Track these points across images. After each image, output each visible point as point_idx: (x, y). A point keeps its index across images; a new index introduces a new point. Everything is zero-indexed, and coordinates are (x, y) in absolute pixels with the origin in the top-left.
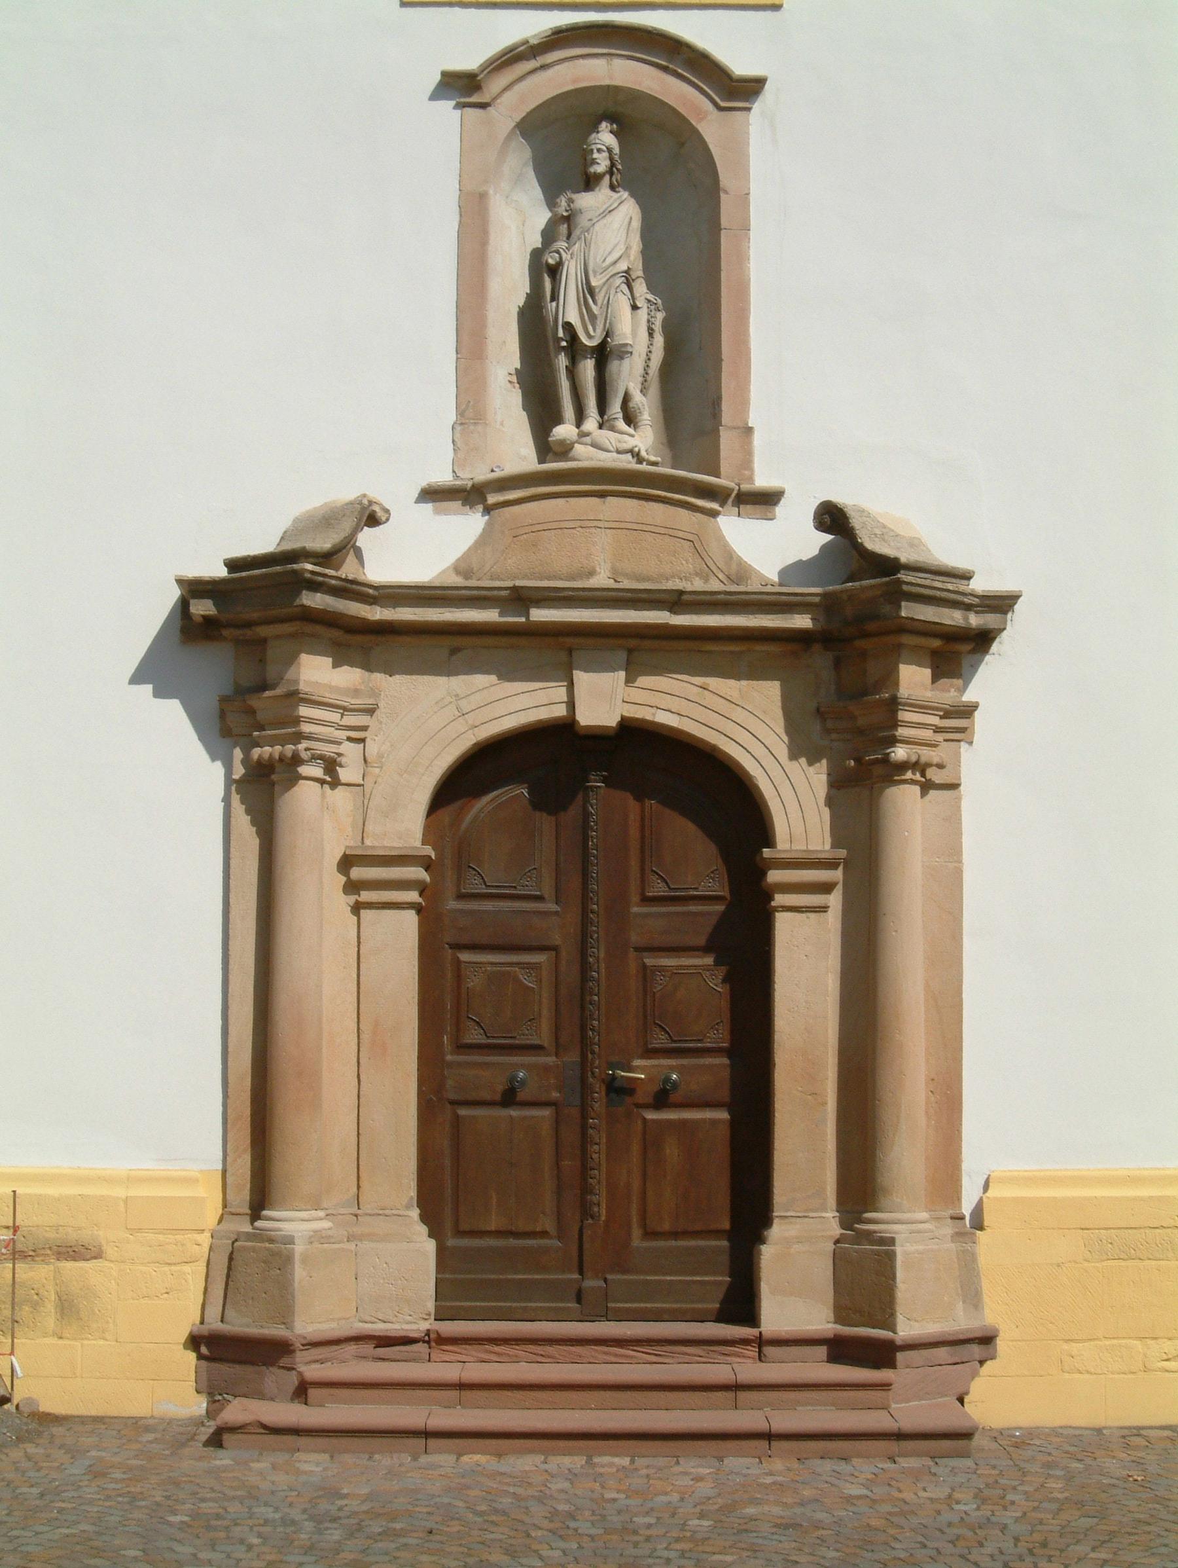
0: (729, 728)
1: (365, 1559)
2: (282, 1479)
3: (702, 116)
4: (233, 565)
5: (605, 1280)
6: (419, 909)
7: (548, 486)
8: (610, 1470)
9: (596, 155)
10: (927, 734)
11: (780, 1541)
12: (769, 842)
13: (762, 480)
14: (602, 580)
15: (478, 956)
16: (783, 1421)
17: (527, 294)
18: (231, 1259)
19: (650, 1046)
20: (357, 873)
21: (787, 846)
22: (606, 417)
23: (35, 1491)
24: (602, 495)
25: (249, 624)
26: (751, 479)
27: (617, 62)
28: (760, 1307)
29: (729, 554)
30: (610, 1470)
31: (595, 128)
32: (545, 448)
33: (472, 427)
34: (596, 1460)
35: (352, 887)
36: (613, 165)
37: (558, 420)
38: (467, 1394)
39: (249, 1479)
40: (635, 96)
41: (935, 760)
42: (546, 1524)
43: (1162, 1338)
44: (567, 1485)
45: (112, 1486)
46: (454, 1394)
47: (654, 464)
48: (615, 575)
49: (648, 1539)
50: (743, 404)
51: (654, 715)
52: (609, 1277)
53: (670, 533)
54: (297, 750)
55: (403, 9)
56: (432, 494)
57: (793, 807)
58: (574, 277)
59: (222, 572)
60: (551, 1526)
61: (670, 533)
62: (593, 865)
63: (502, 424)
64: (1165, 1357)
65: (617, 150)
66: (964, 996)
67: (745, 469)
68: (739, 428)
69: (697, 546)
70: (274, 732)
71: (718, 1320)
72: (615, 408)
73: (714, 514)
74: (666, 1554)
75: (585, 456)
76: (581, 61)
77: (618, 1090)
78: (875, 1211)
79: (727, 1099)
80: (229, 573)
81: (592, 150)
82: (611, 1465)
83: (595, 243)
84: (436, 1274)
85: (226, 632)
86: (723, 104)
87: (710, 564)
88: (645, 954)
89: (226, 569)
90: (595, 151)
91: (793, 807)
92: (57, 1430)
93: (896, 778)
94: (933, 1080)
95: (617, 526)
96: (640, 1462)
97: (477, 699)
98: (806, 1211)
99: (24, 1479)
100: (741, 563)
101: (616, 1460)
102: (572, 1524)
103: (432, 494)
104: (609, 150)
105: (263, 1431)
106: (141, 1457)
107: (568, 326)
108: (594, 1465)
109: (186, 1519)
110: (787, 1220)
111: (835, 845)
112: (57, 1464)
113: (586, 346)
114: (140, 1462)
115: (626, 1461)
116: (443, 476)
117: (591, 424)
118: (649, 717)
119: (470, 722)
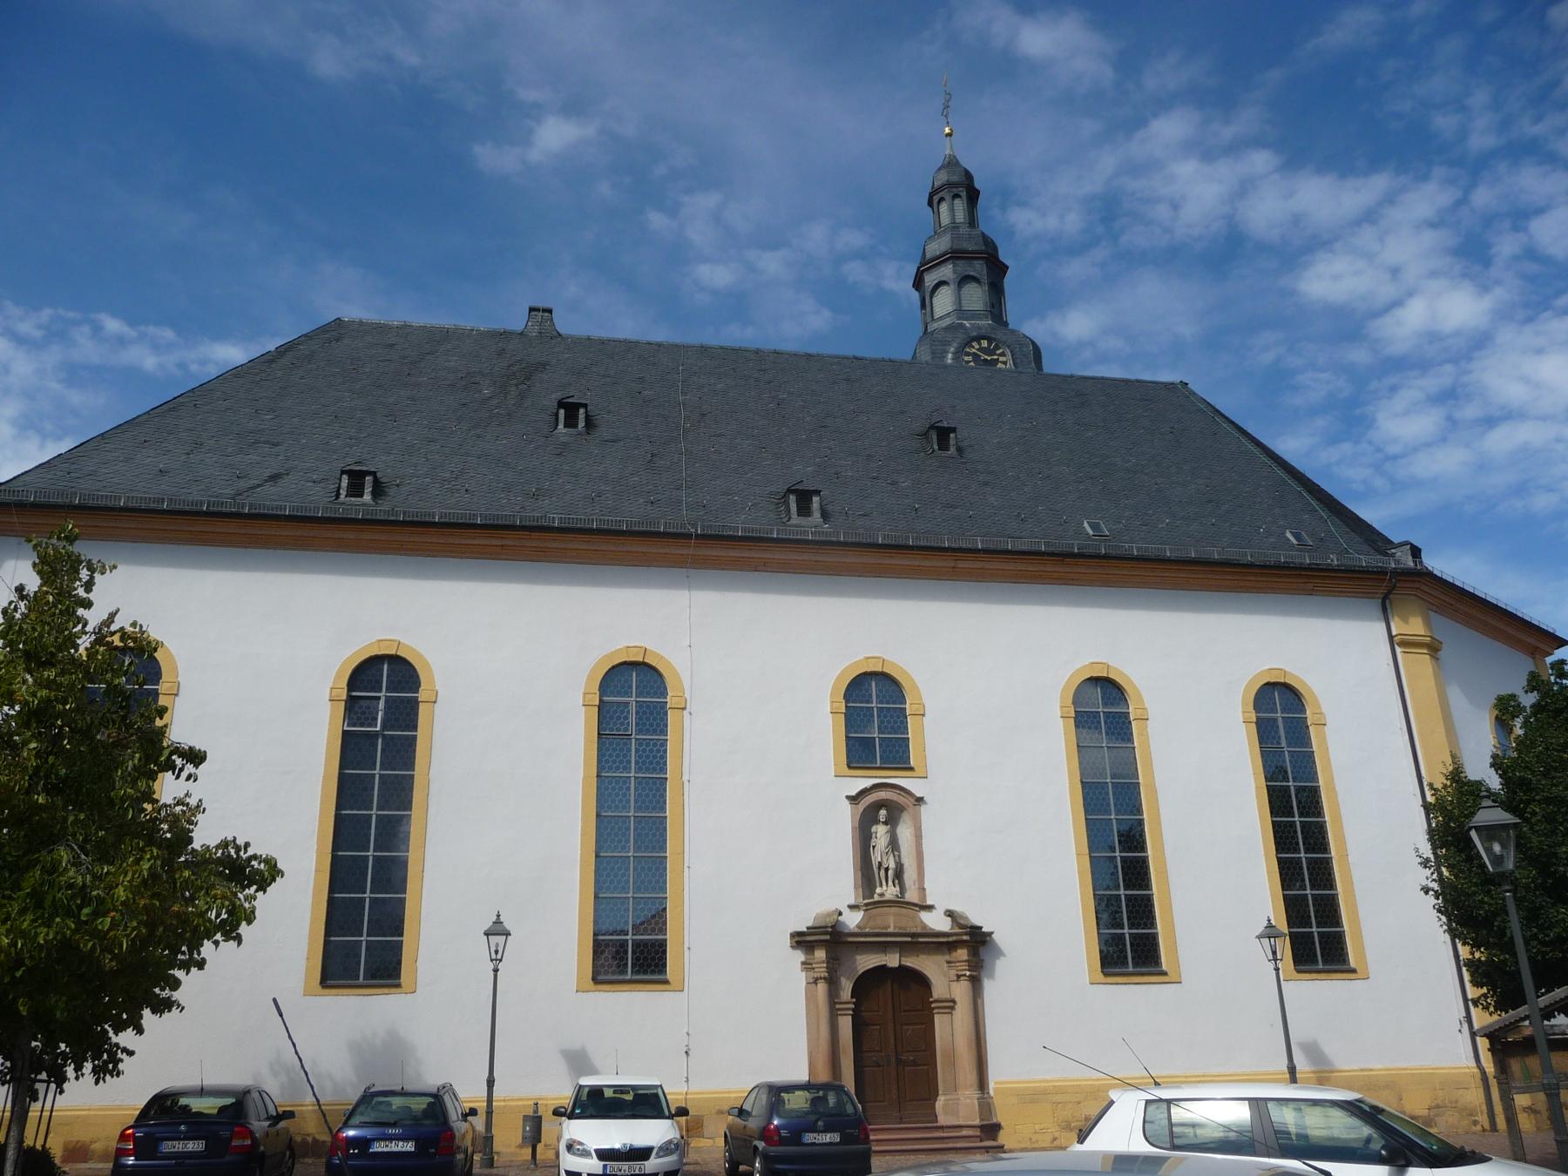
4: (808, 928)
13: (929, 902)
14: (891, 930)
16: (958, 1145)
17: (981, 928)
22: (337, 485)
24: (890, 906)
26: (926, 902)
29: (922, 922)
56: (851, 907)
84: (1283, 889)
97: (864, 960)
111: (852, 997)
116: (852, 902)
117: (884, 888)
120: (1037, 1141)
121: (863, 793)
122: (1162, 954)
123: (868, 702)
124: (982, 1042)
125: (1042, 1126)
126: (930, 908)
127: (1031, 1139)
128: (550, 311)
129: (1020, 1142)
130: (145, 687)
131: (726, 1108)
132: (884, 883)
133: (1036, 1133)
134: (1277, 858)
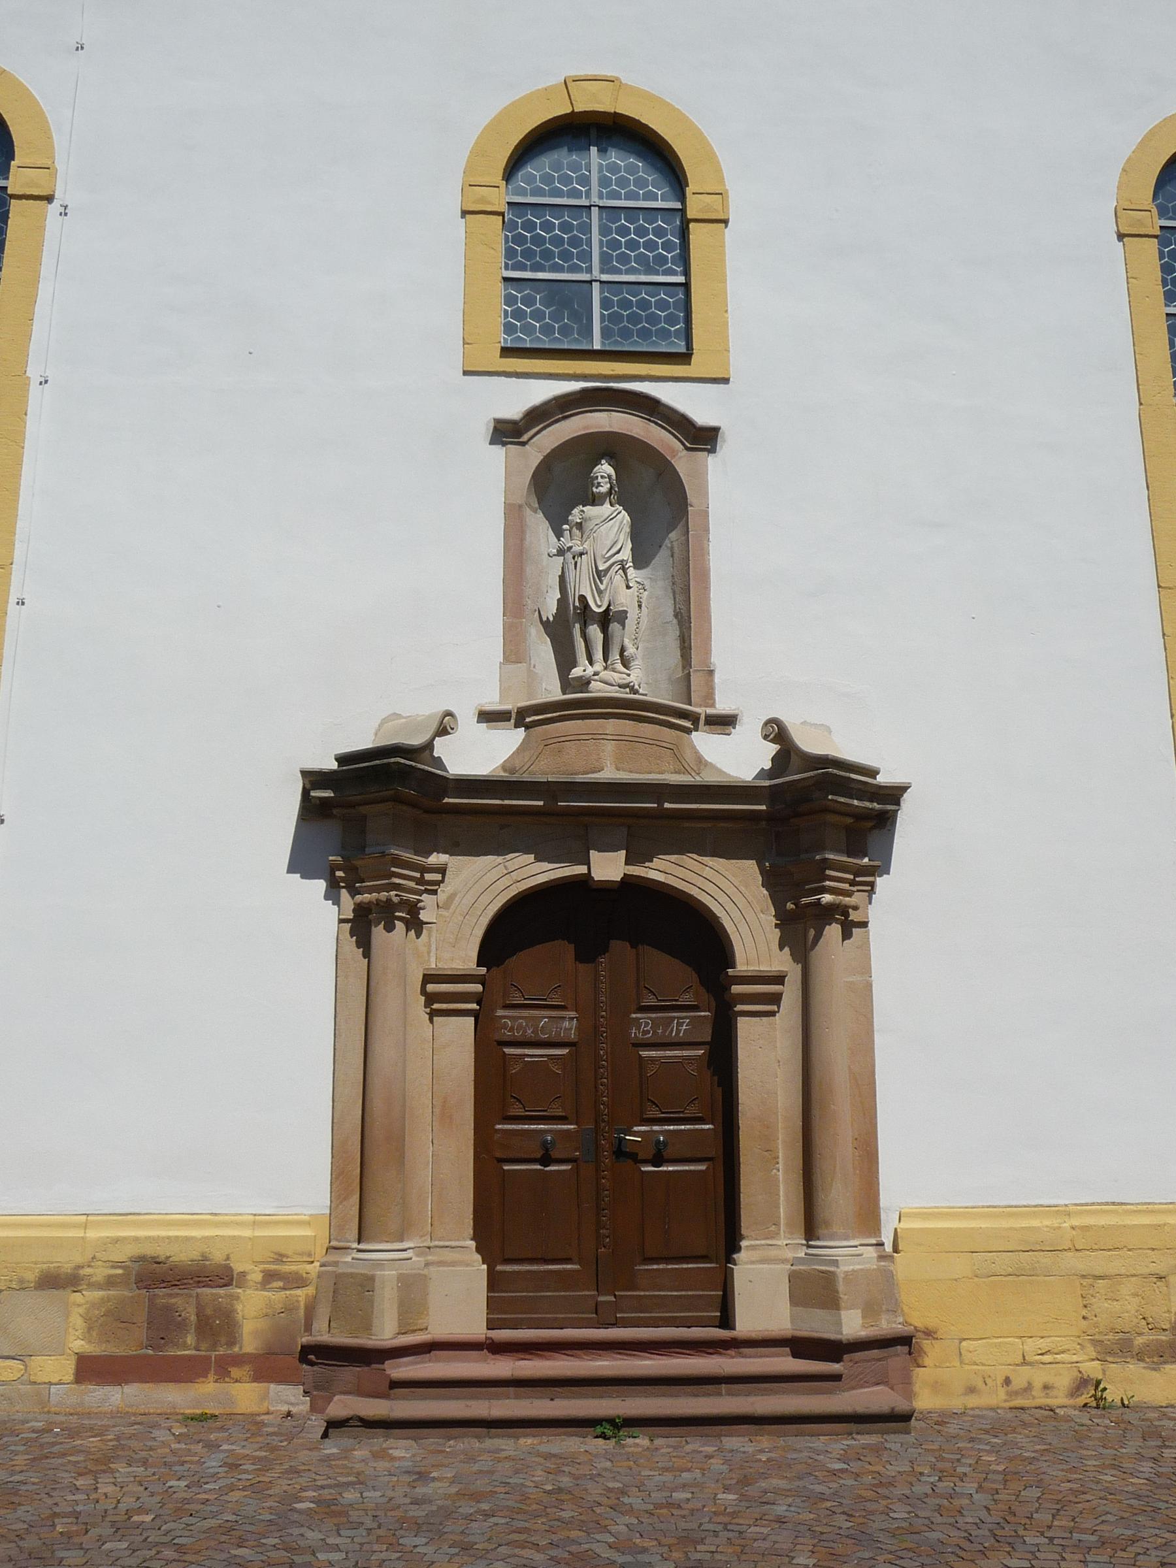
0: (700, 882)
1: (465, 1540)
3: (674, 453)
4: (342, 759)
5: (615, 1296)
6: (476, 1015)
9: (600, 480)
10: (846, 886)
11: (799, 1513)
12: (733, 966)
13: (722, 706)
15: (551, 1050)
19: (645, 1116)
20: (431, 987)
21: (744, 968)
22: (609, 662)
23: (183, 1483)
25: (352, 806)
31: (598, 463)
32: (567, 684)
35: (430, 999)
36: (611, 488)
37: (574, 664)
39: (355, 1465)
41: (853, 903)
42: (604, 1500)
43: (1036, 1337)
44: (609, 1464)
47: (646, 695)
49: (692, 1512)
50: (707, 651)
51: (647, 873)
52: (617, 1293)
53: (656, 743)
54: (390, 895)
55: (466, 377)
56: (488, 717)
57: (748, 940)
59: (334, 765)
60: (610, 1502)
61: (656, 743)
63: (534, 667)
64: (1040, 1352)
65: (614, 477)
66: (876, 1077)
67: (709, 699)
69: (675, 752)
70: (371, 883)
71: (719, 1327)
72: (615, 656)
73: (688, 731)
74: (711, 1527)
75: (598, 689)
76: (589, 414)
77: (622, 1152)
78: (818, 1239)
80: (339, 767)
81: (597, 477)
83: (601, 540)
85: (335, 811)
86: (689, 445)
87: (686, 766)
88: (640, 1048)
89: (337, 763)
90: (599, 478)
91: (748, 940)
94: (856, 1139)
95: (619, 739)
96: (659, 1442)
99: (172, 1473)
102: (626, 1500)
104: (609, 477)
105: (359, 1424)
106: (265, 1449)
107: (583, 598)
108: (624, 1446)
109: (312, 1505)
112: (198, 1458)
113: (594, 612)
114: (265, 1454)
116: (493, 702)
117: (598, 666)
119: (515, 878)
120: (1029, 1388)
121: (540, 416)
122: (712, 591)
123: (605, 259)
124: (512, 1121)
125: (1043, 1344)
126: (724, 722)
127: (1007, 1381)
128: (466, 373)
129: (971, 1390)
130: (446, 800)
131: (31, 1276)
132: (598, 655)
133: (1025, 1363)
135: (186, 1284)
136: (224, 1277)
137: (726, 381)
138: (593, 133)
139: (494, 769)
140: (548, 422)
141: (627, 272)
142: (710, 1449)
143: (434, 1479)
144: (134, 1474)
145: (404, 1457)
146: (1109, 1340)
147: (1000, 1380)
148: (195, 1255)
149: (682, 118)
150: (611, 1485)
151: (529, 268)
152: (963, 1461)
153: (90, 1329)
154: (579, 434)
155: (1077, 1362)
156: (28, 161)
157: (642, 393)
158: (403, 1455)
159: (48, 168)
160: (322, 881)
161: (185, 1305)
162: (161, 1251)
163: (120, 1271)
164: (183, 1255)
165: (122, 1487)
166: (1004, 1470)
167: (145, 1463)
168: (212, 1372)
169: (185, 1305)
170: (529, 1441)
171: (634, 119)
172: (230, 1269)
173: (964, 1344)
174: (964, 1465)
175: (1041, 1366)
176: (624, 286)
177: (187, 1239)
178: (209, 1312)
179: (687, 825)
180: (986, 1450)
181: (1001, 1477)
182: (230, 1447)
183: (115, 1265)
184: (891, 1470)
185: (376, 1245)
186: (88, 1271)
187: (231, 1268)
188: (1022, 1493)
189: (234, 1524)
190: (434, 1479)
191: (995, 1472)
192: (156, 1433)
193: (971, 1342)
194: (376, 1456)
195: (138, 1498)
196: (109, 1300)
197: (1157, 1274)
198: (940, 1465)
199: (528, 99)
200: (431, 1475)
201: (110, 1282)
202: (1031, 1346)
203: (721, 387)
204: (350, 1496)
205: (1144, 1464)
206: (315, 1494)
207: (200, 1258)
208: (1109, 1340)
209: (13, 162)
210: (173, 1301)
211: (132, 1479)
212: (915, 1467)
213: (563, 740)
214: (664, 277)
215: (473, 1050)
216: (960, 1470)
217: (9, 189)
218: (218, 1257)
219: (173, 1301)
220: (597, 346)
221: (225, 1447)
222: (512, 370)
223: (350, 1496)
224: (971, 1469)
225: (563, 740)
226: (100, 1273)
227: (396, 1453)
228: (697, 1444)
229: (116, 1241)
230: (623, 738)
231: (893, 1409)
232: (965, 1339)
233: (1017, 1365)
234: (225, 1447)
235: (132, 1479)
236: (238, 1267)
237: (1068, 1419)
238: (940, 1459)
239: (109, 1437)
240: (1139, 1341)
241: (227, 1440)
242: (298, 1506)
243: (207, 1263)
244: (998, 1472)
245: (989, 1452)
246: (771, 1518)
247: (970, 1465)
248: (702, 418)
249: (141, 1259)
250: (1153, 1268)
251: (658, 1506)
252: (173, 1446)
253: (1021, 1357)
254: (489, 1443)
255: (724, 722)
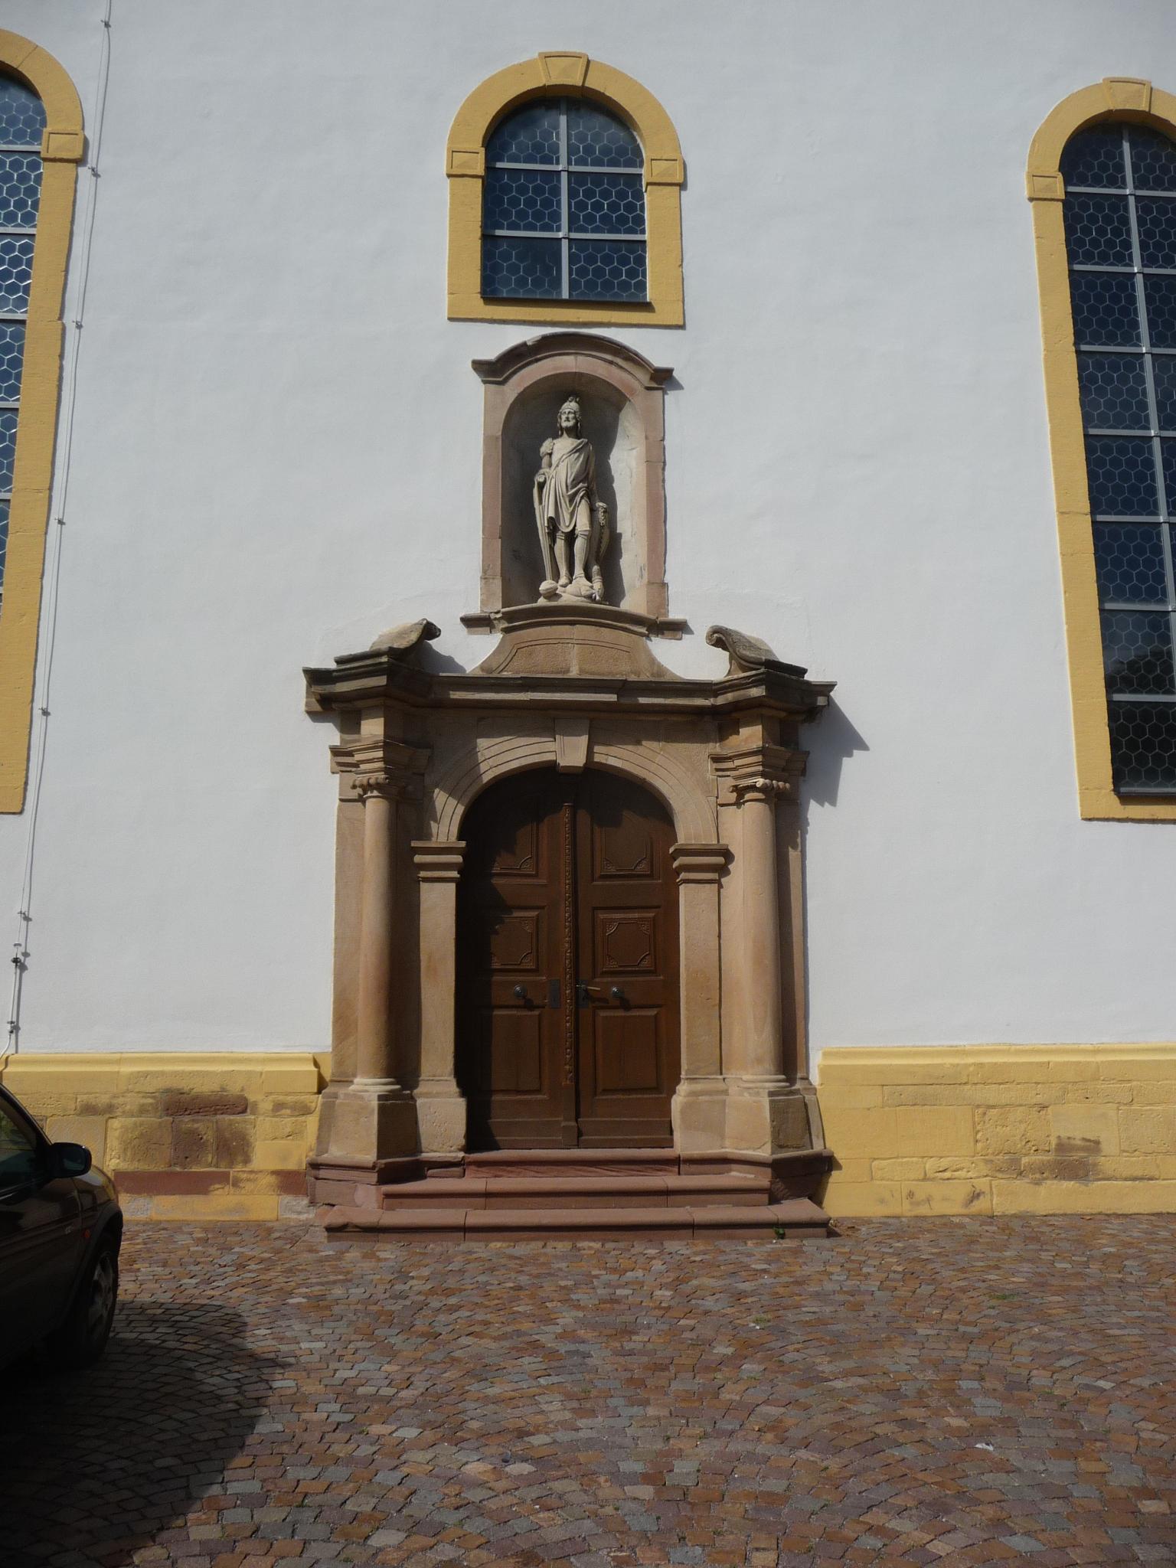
2: (367, 1265)
4: (339, 661)
7: (564, 692)
8: (589, 1252)
13: (674, 614)
14: (574, 673)
18: (1090, 820)
23: (194, 1281)
24: (572, 623)
27: (580, 358)
28: (548, 307)
29: (653, 661)
30: (589, 1252)
33: (491, 581)
34: (580, 1245)
38: (493, 1200)
40: (593, 380)
45: (250, 1275)
46: (482, 1200)
48: (581, 671)
51: (607, 760)
56: (470, 622)
58: (554, 494)
62: (569, 849)
68: (657, 583)
79: (586, 85)
82: (590, 1248)
92: (111, 1294)
93: (381, 681)
95: (583, 643)
96: (609, 1245)
98: (708, 1074)
100: (660, 666)
101: (592, 1244)
103: (470, 622)
110: (695, 1081)
115: (597, 1245)
116: (475, 609)
118: (604, 761)
119: (491, 764)
121: (518, 357)
125: (944, 1163)
126: (677, 628)
127: (911, 1194)
128: (450, 319)
132: (563, 570)
133: (925, 1179)
134: (1078, 352)
135: (206, 1111)
136: (240, 1106)
137: (682, 327)
138: (563, 107)
139: (474, 669)
140: (522, 363)
141: (594, 231)
142: (652, 1252)
143: (413, 1278)
144: (154, 1273)
145: (389, 1258)
146: (999, 1160)
147: (905, 1193)
148: (216, 1087)
149: (642, 91)
150: (563, 1283)
151: (522, 227)
152: (869, 1262)
153: (125, 1150)
154: (550, 374)
155: (971, 1178)
156: (59, 127)
157: (605, 337)
158: (388, 1257)
159: (76, 134)
160: (735, 800)
161: (205, 1127)
162: (184, 1085)
163: (150, 1101)
164: (205, 1088)
165: (141, 1285)
166: (904, 1270)
167: (165, 1265)
168: (418, 1157)
169: (205, 1127)
170: (499, 1244)
171: (597, 91)
172: (246, 1099)
173: (876, 1163)
174: (869, 1266)
175: (941, 1181)
176: (607, 243)
177: (207, 1073)
178: (227, 1135)
179: (643, 718)
180: (889, 1253)
181: (899, 1276)
182: (242, 1250)
183: (147, 1095)
184: (807, 1270)
185: (604, 353)
186: (121, 1100)
187: (245, 1098)
188: (918, 1291)
189: (234, 1316)
190: (413, 1278)
191: (895, 1272)
192: (179, 1237)
193: (882, 1161)
194: (365, 1256)
195: (153, 1295)
196: (141, 1124)
197: (1040, 1104)
198: (847, 1266)
199: (503, 74)
200: (411, 1275)
201: (142, 1110)
202: (930, 1165)
203: (680, 332)
204: (338, 1292)
205: (1024, 1265)
206: (307, 1290)
207: (219, 1090)
208: (999, 1160)
209: (45, 130)
210: (196, 1126)
211: (151, 1277)
212: (827, 1267)
213: (533, 644)
214: (524, 232)
215: (454, 912)
216: (865, 1270)
217: (42, 153)
218: (234, 1089)
219: (196, 1126)
220: (565, 295)
221: (237, 1249)
222: (489, 317)
223: (338, 1292)
224: (876, 1269)
225: (533, 644)
226: (132, 1102)
227: (382, 1255)
228: (642, 1248)
229: (146, 1074)
230: (587, 642)
231: (811, 1218)
232: (875, 1159)
233: (919, 1180)
234: (237, 1249)
235: (151, 1277)
236: (252, 1097)
237: (962, 1226)
238: (849, 1260)
239: (138, 1241)
240: (1025, 1160)
241: (241, 1243)
242: (291, 1301)
243: (225, 1093)
244: (898, 1272)
245: (893, 1255)
246: (699, 1311)
247: (875, 1267)
248: (659, 362)
249: (168, 1091)
250: (1039, 1099)
251: (602, 1301)
252: (192, 1249)
253: (923, 1174)
254: (464, 1247)
255: (677, 628)
